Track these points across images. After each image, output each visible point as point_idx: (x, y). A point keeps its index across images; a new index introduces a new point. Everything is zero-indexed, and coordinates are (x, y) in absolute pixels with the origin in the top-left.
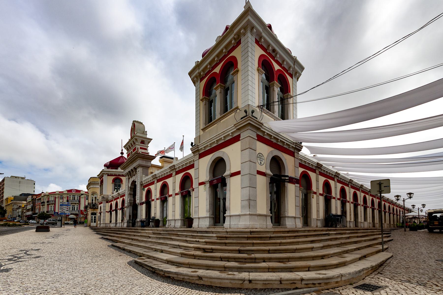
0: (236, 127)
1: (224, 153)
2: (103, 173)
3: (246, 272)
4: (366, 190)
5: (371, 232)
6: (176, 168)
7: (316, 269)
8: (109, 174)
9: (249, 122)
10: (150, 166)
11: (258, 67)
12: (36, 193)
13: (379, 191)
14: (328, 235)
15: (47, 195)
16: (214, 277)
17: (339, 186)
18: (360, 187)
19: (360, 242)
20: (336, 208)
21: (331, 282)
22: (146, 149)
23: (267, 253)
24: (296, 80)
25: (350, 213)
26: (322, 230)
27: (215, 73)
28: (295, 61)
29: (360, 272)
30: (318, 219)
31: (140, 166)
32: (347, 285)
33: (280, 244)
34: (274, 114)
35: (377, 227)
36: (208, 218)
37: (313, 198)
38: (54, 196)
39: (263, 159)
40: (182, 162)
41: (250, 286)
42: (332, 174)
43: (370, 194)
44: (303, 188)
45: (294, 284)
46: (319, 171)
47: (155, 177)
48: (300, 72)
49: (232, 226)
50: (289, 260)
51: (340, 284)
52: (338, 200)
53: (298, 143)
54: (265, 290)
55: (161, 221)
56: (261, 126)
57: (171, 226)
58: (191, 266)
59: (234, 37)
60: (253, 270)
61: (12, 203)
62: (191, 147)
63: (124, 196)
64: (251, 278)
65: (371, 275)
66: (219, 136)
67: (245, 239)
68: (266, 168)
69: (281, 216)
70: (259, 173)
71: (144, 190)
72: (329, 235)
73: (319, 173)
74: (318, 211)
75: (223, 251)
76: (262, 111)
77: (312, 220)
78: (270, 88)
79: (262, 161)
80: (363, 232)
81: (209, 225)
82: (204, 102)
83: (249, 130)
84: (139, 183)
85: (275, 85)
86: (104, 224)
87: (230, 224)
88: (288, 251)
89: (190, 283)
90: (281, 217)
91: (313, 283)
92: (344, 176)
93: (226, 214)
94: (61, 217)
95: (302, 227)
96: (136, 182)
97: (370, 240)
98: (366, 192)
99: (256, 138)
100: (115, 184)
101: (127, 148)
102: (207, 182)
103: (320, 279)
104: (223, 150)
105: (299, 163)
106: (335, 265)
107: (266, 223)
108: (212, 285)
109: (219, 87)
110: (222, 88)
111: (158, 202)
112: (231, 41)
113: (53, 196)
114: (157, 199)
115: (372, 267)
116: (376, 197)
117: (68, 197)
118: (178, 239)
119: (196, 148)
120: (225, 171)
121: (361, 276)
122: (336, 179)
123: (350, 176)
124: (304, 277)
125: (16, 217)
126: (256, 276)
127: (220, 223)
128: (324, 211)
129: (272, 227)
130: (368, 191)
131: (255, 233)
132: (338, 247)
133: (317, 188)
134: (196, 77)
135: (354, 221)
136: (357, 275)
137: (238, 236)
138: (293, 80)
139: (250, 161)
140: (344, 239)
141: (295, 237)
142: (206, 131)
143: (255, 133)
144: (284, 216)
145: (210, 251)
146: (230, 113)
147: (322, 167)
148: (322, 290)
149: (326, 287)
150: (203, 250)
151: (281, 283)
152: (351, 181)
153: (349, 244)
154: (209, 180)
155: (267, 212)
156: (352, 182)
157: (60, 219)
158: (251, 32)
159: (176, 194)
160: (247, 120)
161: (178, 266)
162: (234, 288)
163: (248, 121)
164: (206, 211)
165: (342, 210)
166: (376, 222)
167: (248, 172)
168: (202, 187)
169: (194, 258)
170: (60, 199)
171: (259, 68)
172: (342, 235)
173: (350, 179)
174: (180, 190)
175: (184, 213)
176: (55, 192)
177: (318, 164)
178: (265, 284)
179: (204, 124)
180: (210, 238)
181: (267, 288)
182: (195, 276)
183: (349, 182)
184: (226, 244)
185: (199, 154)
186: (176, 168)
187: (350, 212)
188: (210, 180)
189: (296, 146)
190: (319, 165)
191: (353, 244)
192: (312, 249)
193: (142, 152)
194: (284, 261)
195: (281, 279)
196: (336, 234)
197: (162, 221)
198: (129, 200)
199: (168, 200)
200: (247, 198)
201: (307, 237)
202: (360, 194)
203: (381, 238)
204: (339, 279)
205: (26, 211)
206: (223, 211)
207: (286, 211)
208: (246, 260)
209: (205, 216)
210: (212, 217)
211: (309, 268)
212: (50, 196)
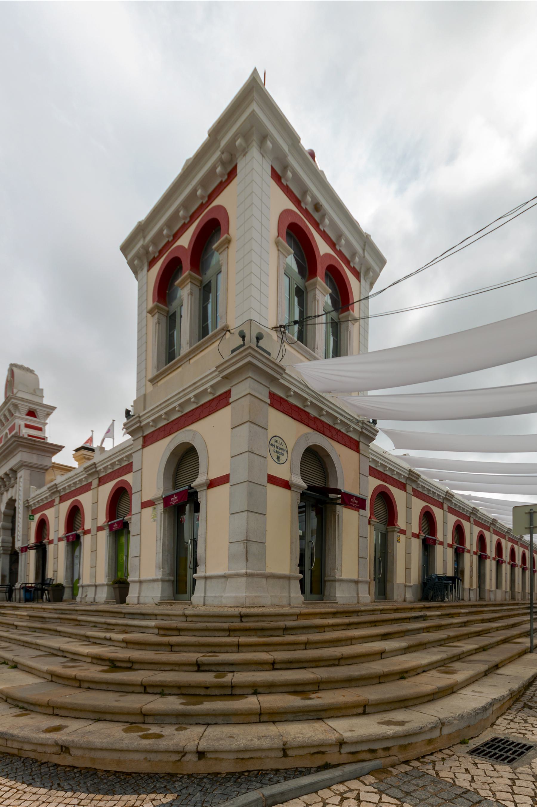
0: (221, 372)
1: (195, 433)
3: (200, 724)
4: (502, 529)
5: (508, 609)
6: (98, 469)
7: (384, 707)
9: (249, 359)
10: (50, 467)
11: (278, 236)
13: (530, 528)
14: (424, 618)
17: (452, 519)
18: (491, 523)
19: (486, 632)
20: (445, 562)
21: (416, 743)
22: (40, 429)
24: (368, 286)
25: (470, 572)
26: (412, 609)
27: (181, 247)
29: (484, 709)
30: (407, 584)
31: (23, 465)
32: (453, 745)
33: (307, 645)
34: (315, 353)
35: (518, 600)
36: (160, 583)
37: (399, 542)
39: (284, 450)
41: (202, 767)
42: (439, 496)
43: (508, 537)
44: (378, 521)
45: (319, 756)
46: (413, 488)
47: (54, 490)
48: (377, 269)
49: (209, 601)
50: (319, 687)
51: (438, 745)
52: (448, 546)
53: (368, 424)
54: (239, 777)
55: (69, 587)
56: (281, 374)
57: (87, 599)
58: (56, 711)
59: (221, 157)
60: (219, 720)
62: (125, 420)
64: (203, 745)
65: (509, 711)
66: (185, 395)
67: (223, 633)
68: (291, 471)
69: (326, 579)
70: (273, 480)
71: (33, 519)
72: (425, 618)
73: (413, 491)
74: (408, 569)
75: (159, 666)
76: (282, 339)
77: (395, 587)
78: (307, 293)
79: (282, 454)
80: (493, 612)
81: (161, 597)
82: (156, 316)
83: (249, 379)
84: (21, 503)
87: (205, 597)
88: (321, 664)
89: (37, 761)
90: (325, 581)
92: (463, 500)
93: (196, 573)
95: (374, 602)
97: (508, 627)
98: (502, 532)
99: (269, 401)
102: (158, 499)
103: (387, 738)
104: (197, 427)
105: (370, 466)
106: (428, 695)
107: (289, 593)
108: (97, 767)
109: (187, 280)
111: (63, 545)
112: (213, 169)
114: (60, 540)
115: (511, 694)
116: (519, 543)
120: (196, 476)
121: (488, 717)
122: (445, 506)
123: (473, 501)
124: (347, 735)
126: (219, 739)
127: (186, 593)
128: (421, 569)
129: (303, 603)
130: (504, 531)
132: (440, 645)
133: (408, 523)
134: (137, 256)
135: (478, 589)
136: (480, 717)
138: (360, 284)
139: (252, 452)
140: (455, 626)
141: (348, 626)
142: (160, 384)
143: (265, 388)
144: (332, 578)
145: (125, 665)
147: (420, 479)
148: (393, 766)
149: (402, 757)
150: (110, 664)
151: (285, 755)
152: (474, 511)
153: (465, 639)
154: (162, 496)
156: (477, 512)
159: (100, 529)
160: (244, 354)
161: (27, 710)
162: (157, 774)
163: (246, 356)
164: (156, 567)
165: (456, 567)
166: (516, 590)
167: (245, 478)
168: (148, 511)
169: (78, 684)
171: (280, 238)
172: (452, 617)
173: (474, 508)
174: (107, 519)
175: (115, 571)
177: (412, 473)
178: (242, 759)
180: (143, 630)
181: (247, 771)
182: (49, 742)
183: (471, 513)
184: (171, 647)
185: (142, 436)
187: (471, 571)
188: (164, 497)
189: (362, 428)
190: (412, 475)
191: (473, 637)
192: (381, 654)
193: (29, 436)
194: (305, 690)
195: (284, 745)
196: (440, 617)
197: (70, 589)
199: (82, 541)
200: (243, 537)
201: (375, 626)
202: (491, 538)
203: (530, 622)
204: (436, 734)
206: (192, 567)
207: (336, 568)
208: (209, 689)
209: (155, 577)
210: (169, 581)
211: (365, 706)
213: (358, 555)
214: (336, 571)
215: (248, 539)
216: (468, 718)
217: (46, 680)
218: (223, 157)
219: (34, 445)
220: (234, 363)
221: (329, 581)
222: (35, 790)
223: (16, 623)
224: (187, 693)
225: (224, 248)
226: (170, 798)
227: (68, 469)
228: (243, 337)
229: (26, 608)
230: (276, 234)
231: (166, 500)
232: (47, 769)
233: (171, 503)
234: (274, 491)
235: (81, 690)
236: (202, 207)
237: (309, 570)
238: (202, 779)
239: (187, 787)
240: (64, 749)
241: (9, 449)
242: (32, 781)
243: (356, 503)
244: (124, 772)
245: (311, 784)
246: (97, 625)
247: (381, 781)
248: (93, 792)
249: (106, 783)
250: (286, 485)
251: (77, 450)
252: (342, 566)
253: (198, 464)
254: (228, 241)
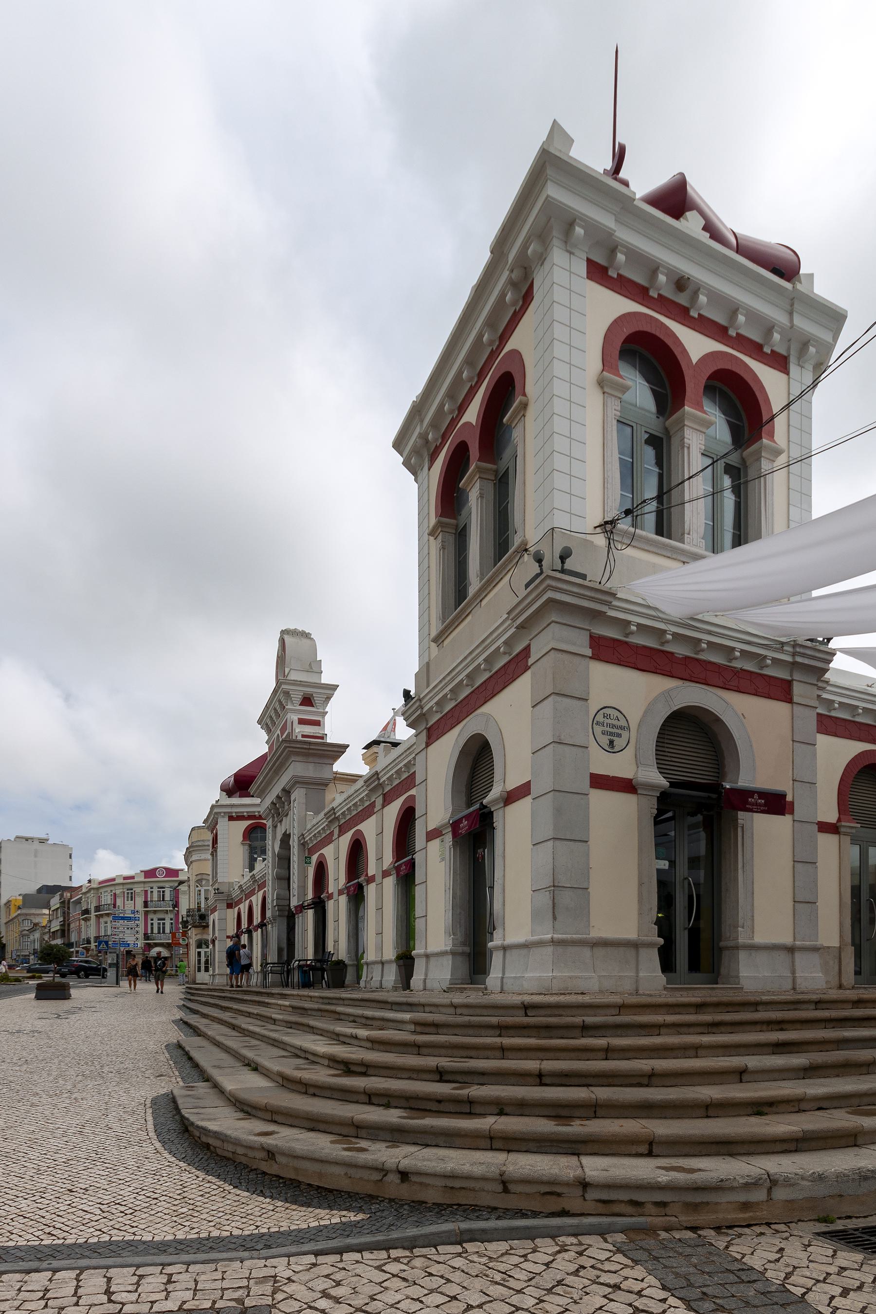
0: (514, 620)
1: (488, 717)
2: (216, 813)
6: (381, 781)
8: (232, 813)
9: (550, 594)
11: (603, 370)
12: (75, 884)
15: (93, 889)
22: (317, 723)
23: (436, 1079)
27: (467, 424)
28: (793, 299)
31: (298, 782)
32: (799, 1221)
36: (450, 957)
38: (111, 891)
39: (622, 728)
40: (395, 760)
41: (404, 1191)
45: (553, 1198)
47: (332, 817)
48: (826, 336)
50: (595, 1112)
54: (445, 1209)
56: (608, 604)
58: (275, 1117)
61: (19, 915)
64: (405, 1164)
67: (492, 1032)
69: (722, 944)
70: (600, 782)
79: (619, 736)
83: (553, 624)
85: (686, 423)
86: (221, 975)
87: (502, 978)
89: (248, 1167)
91: (635, 1198)
94: (115, 955)
100: (250, 846)
101: (267, 724)
102: (444, 826)
104: (486, 709)
109: (475, 476)
110: (485, 477)
111: (343, 900)
113: (109, 889)
117: (146, 892)
118: (323, 1030)
125: (29, 956)
129: (665, 989)
131: (542, 1012)
137: (469, 1021)
142: (446, 643)
146: (504, 569)
148: (667, 1230)
149: (685, 1219)
151: (506, 1190)
155: (640, 930)
157: (115, 962)
158: (566, 242)
160: (541, 588)
161: (250, 1115)
162: (358, 1194)
163: (544, 591)
168: (435, 844)
169: (304, 1090)
170: (126, 898)
175: (407, 938)
176: (114, 880)
178: (452, 1188)
185: (426, 728)
186: (381, 781)
188: (451, 822)
189: (794, 655)
193: (303, 736)
195: (501, 1175)
198: (277, 899)
200: (548, 882)
204: (759, 1195)
205: (50, 937)
207: (740, 923)
208: (443, 1103)
210: (462, 954)
212: (102, 890)
213: (794, 898)
214: (739, 929)
215: (556, 884)
216: (837, 1181)
217: (277, 1084)
218: (513, 276)
219: (309, 749)
220: (529, 603)
221: (727, 948)
222: (239, 1192)
223: (274, 1016)
224: (416, 1107)
225: (519, 417)
226: (360, 1216)
227: (351, 779)
228: (539, 561)
229: (293, 995)
230: (600, 366)
231: (455, 826)
232: (255, 1176)
233: (460, 831)
234: (600, 799)
235: (306, 1096)
236: (493, 355)
237: (685, 929)
238: (403, 1205)
239: (384, 1210)
240: (271, 1154)
242: (239, 1184)
243: (760, 805)
244: (326, 1188)
245: (527, 1228)
246: (357, 1019)
247: (632, 1241)
248: (291, 1202)
249: (306, 1196)
250: (627, 786)
251: (368, 747)
252: (753, 920)
253: (491, 764)
254: (525, 406)
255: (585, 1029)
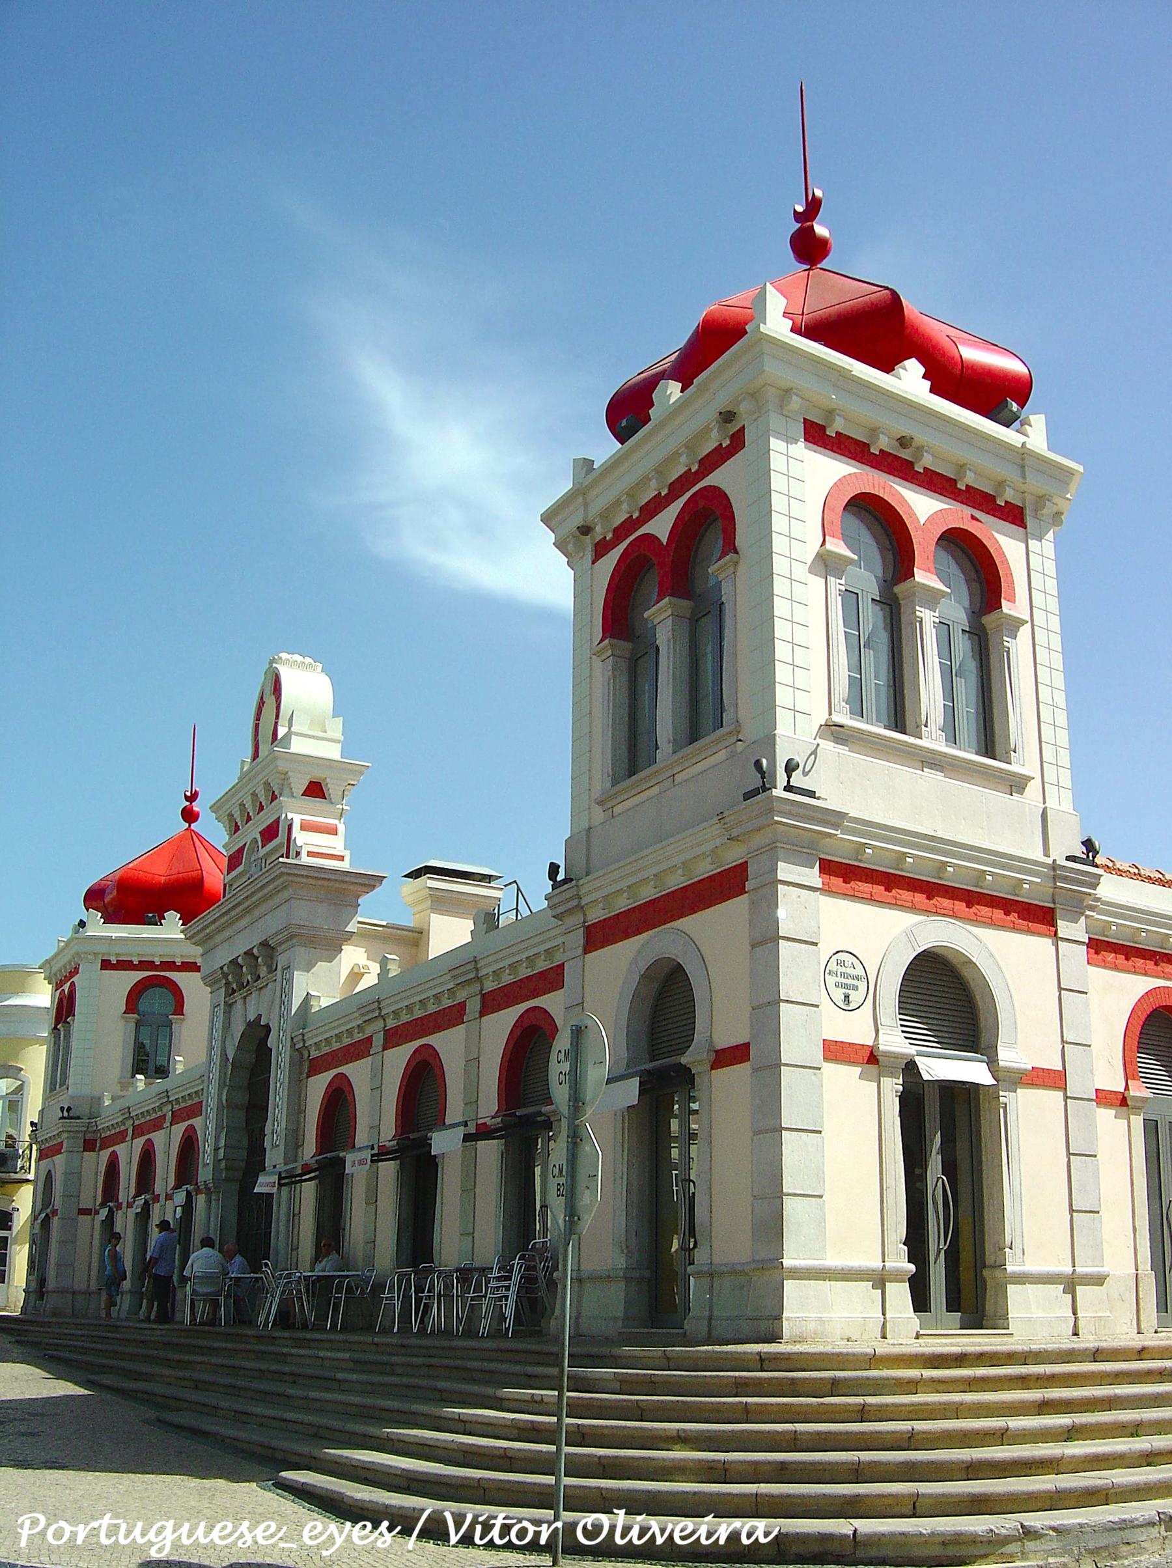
16: (293, 1420)
27: (650, 538)
39: (858, 978)
63: (195, 1110)
79: (856, 988)
87: (710, 1319)
96: (268, 1028)
101: (231, 815)
104: (687, 923)
119: (571, 898)
179: (609, 776)
207: (1008, 1242)
241: (266, 891)
255: (835, 1388)
